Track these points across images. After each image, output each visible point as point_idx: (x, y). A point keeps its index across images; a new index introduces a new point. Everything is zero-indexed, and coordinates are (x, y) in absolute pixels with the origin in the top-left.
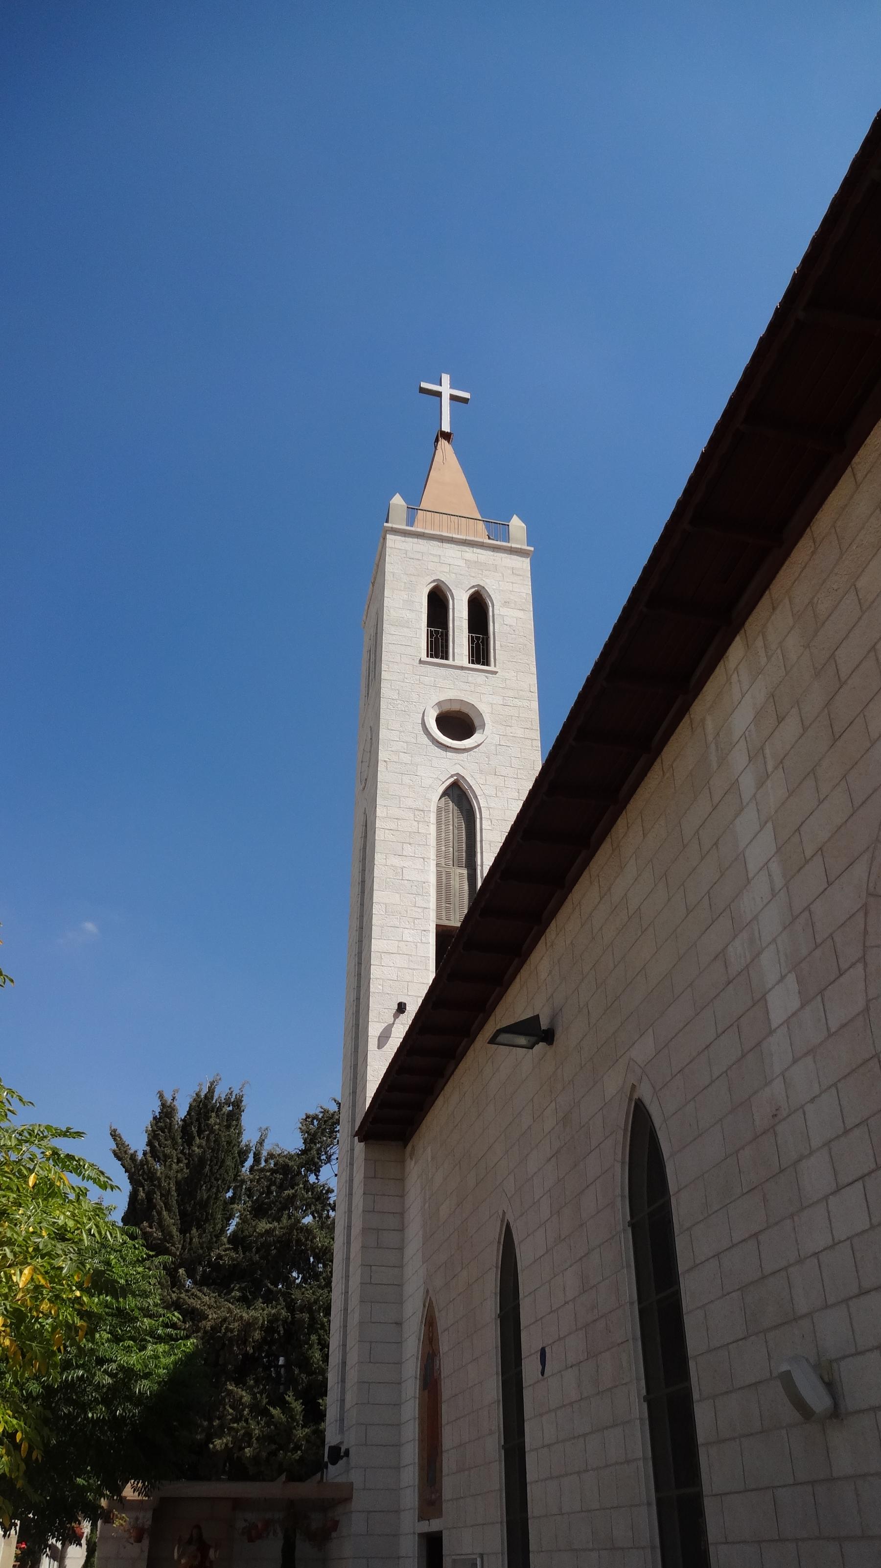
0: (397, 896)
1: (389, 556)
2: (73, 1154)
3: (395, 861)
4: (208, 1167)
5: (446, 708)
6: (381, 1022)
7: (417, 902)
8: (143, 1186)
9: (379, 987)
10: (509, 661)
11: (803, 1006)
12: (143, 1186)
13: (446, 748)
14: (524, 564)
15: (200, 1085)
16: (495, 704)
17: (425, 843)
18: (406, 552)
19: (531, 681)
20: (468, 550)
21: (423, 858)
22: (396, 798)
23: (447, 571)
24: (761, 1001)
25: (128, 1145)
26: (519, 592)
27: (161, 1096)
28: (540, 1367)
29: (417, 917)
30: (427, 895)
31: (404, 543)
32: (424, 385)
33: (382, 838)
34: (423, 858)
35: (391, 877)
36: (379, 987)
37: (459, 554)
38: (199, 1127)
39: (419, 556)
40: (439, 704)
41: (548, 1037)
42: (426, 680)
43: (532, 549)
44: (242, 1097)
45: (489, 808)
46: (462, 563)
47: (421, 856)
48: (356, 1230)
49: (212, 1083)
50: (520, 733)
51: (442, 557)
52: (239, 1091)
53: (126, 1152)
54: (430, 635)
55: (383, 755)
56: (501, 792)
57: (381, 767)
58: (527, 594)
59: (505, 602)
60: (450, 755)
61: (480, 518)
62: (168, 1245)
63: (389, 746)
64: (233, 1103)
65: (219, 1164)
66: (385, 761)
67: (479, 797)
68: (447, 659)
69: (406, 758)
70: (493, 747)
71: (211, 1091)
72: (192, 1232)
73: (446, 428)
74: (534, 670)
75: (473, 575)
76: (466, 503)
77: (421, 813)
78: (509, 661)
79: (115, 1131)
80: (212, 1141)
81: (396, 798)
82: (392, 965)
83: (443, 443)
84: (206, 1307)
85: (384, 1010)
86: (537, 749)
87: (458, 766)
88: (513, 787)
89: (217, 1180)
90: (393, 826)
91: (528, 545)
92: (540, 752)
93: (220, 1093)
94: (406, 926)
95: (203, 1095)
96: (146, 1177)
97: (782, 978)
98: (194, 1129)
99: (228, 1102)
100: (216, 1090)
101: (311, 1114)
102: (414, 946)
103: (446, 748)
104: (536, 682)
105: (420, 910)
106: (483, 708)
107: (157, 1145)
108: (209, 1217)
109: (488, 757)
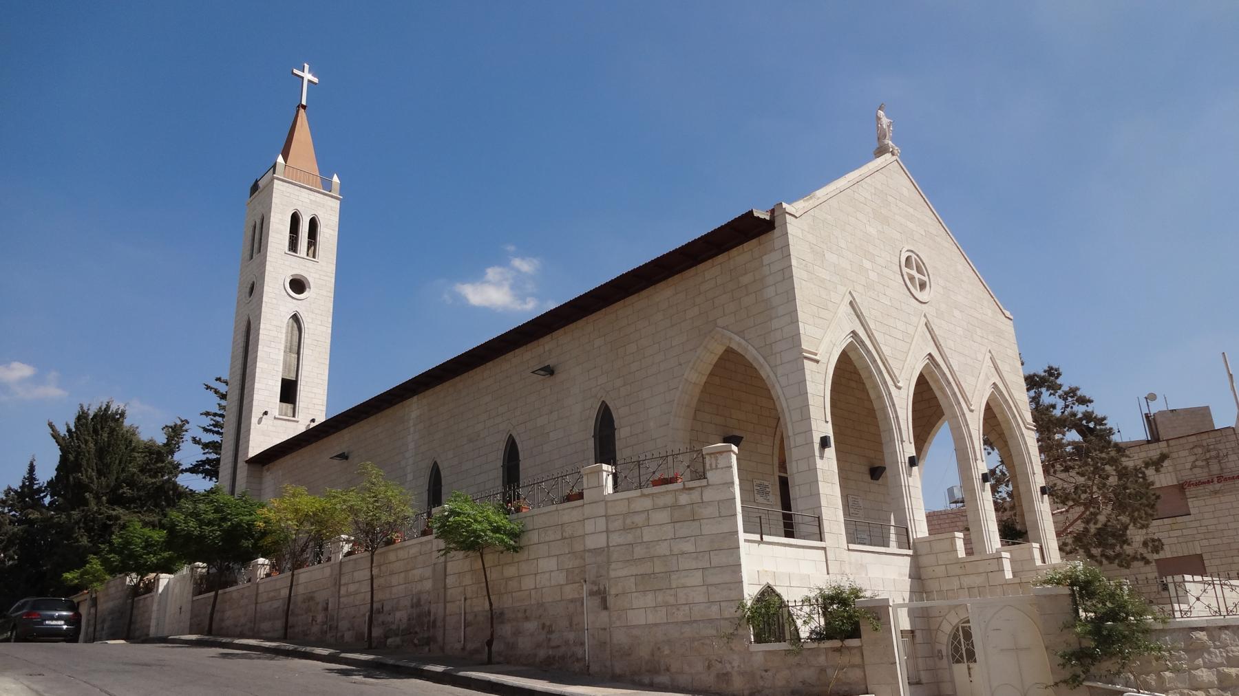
3: (266, 349)
5: (295, 277)
14: (336, 204)
18: (283, 192)
19: (332, 268)
24: (406, 475)
27: (82, 407)
32: (296, 71)
37: (307, 196)
39: (288, 195)
42: (286, 263)
46: (308, 201)
50: (325, 293)
54: (291, 237)
55: (265, 299)
57: (264, 305)
60: (294, 301)
64: (120, 414)
68: (297, 253)
71: (108, 407)
73: (304, 103)
76: (314, 168)
79: (51, 423)
83: (302, 111)
89: (115, 454)
93: (113, 408)
95: (103, 409)
98: (99, 427)
106: (310, 280)
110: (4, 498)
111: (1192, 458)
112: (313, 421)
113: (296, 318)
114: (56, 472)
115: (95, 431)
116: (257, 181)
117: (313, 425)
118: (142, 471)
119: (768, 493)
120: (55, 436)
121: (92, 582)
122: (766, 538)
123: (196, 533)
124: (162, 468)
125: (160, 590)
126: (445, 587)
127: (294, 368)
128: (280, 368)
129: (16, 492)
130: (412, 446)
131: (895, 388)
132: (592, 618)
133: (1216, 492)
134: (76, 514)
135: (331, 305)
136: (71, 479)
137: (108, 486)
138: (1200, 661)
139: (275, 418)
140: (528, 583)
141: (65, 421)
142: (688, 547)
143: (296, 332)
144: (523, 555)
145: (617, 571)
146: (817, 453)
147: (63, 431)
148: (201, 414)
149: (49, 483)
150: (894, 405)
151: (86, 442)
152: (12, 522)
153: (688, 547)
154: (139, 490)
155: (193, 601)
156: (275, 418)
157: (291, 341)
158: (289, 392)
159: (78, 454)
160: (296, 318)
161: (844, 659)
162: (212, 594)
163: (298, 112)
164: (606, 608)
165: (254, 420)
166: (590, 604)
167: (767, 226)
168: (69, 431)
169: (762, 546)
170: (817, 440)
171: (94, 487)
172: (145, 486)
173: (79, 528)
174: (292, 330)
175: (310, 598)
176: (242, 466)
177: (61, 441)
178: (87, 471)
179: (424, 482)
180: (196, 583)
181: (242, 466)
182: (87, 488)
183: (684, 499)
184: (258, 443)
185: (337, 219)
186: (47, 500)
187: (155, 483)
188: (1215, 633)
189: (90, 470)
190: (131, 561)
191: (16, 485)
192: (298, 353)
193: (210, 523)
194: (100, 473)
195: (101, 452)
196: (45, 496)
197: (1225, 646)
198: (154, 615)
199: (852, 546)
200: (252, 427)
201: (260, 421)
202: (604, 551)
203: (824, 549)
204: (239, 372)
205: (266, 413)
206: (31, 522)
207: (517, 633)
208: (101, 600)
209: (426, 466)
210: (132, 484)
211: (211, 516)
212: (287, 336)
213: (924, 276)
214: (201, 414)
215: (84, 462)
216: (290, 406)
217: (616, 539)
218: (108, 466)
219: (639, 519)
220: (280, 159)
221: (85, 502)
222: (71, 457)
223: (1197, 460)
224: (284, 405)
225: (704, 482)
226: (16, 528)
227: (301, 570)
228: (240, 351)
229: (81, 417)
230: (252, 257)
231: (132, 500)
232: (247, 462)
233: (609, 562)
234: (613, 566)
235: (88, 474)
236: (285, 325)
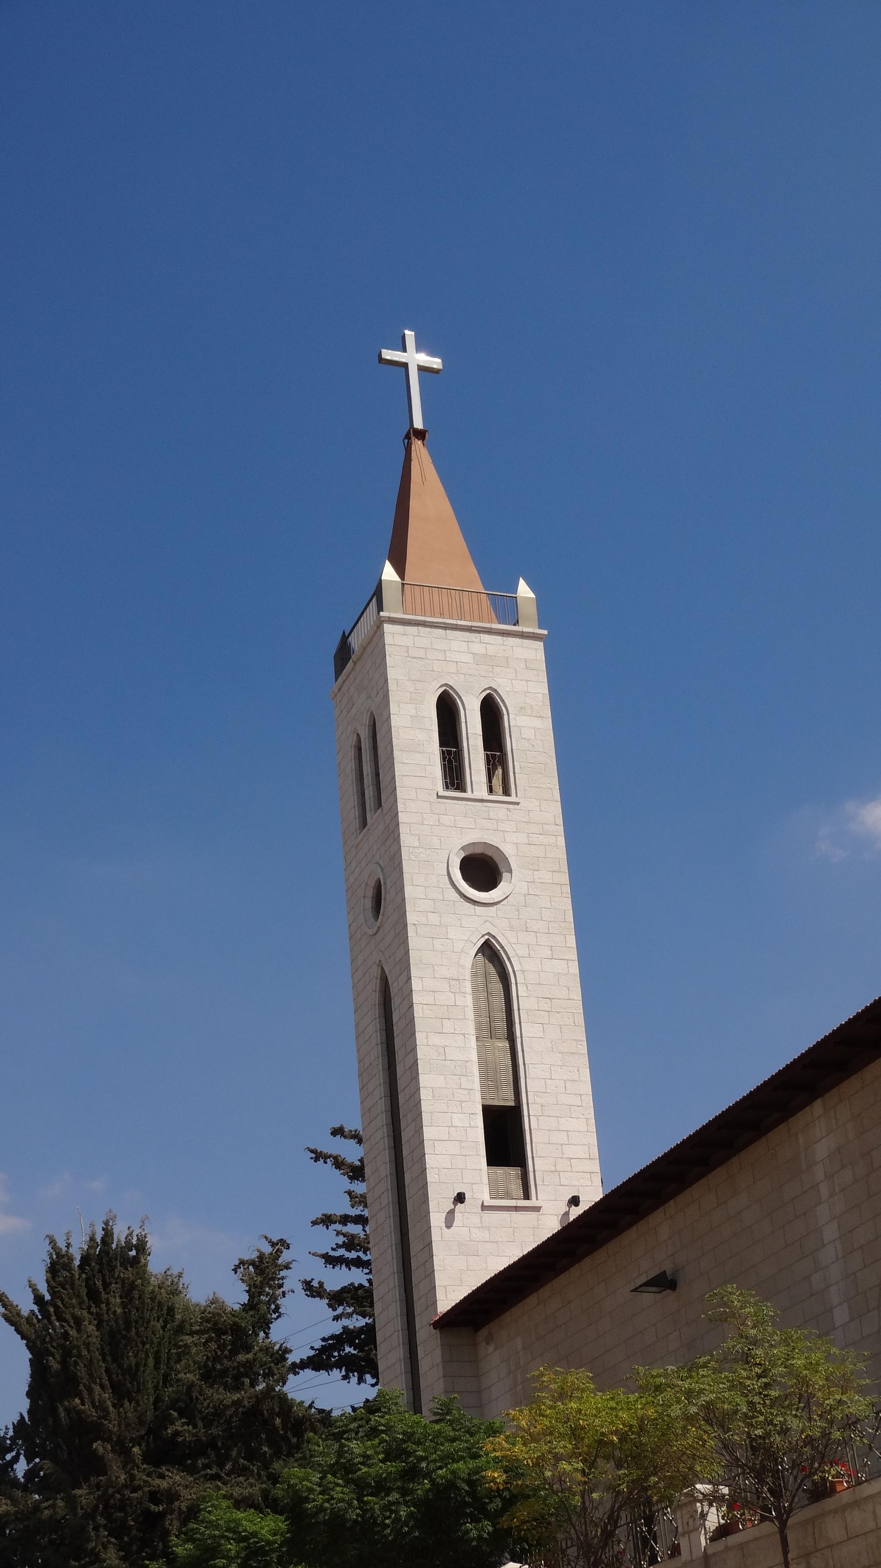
0: (443, 1078)
1: (389, 656)
2: (15, 1332)
3: (435, 1040)
4: (133, 1329)
6: (440, 1212)
7: (462, 1084)
8: (53, 1355)
9: (436, 1176)
10: (530, 787)
11: (850, 1321)
12: (53, 1355)
13: (475, 902)
14: (535, 652)
15: (92, 1225)
16: (519, 844)
17: (462, 1017)
20: (475, 640)
21: (464, 1035)
22: (428, 967)
23: (454, 671)
25: (17, 1306)
26: (535, 693)
27: (53, 1242)
29: (464, 1100)
30: (471, 1075)
31: (404, 637)
32: (388, 354)
33: (421, 1015)
34: (464, 1035)
35: (434, 1058)
36: (436, 1176)
38: (104, 1281)
39: (421, 654)
40: (463, 848)
42: (446, 820)
43: (545, 632)
44: (145, 1237)
45: (523, 971)
46: (469, 658)
47: (460, 1032)
49: (106, 1223)
51: (447, 654)
52: (140, 1230)
53: (18, 1314)
54: (445, 756)
55: (411, 918)
56: (534, 951)
58: (543, 694)
59: (521, 708)
60: (479, 909)
61: (484, 591)
62: (105, 1423)
63: (416, 905)
65: (145, 1325)
66: (414, 924)
67: (511, 959)
68: (465, 791)
69: (434, 919)
70: (522, 898)
72: (125, 1406)
73: (418, 424)
75: (483, 674)
77: (456, 982)
78: (530, 787)
80: (137, 1298)
81: (428, 967)
82: (445, 1152)
84: (180, 1488)
85: (443, 1200)
86: (567, 895)
87: (488, 924)
88: (546, 944)
90: (431, 1001)
91: (540, 627)
92: (570, 899)
93: (120, 1234)
94: (455, 1111)
96: (55, 1344)
97: (840, 1304)
98: (99, 1283)
99: (129, 1246)
100: (114, 1231)
101: (246, 1259)
102: (464, 1131)
103: (475, 902)
104: (561, 812)
105: (465, 1092)
106: (508, 850)
107: (61, 1305)
108: (141, 1387)
109: (518, 910)
112: (574, 1201)
114: (23, 1405)
117: (575, 1212)
118: (208, 1375)
123: (352, 1515)
124: (249, 1364)
128: (475, 1082)
130: (830, 1232)
135: (566, 904)
137: (141, 1422)
139: (484, 1207)
147: (26, 1305)
148: (314, 1223)
151: (78, 1322)
159: (67, 1353)
165: (437, 1219)
168: (39, 1299)
177: (25, 1327)
178: (90, 1391)
181: (424, 1332)
182: (97, 1431)
186: (21, 1467)
187: (237, 1403)
189: (97, 1389)
193: (381, 1487)
194: (120, 1393)
196: (16, 1459)
205: (460, 1198)
212: (476, 1000)
214: (314, 1223)
215: (81, 1371)
216: (513, 1172)
220: (389, 573)
221: (99, 1466)
222: (54, 1364)
224: (500, 1171)
230: (364, 823)
231: (199, 1449)
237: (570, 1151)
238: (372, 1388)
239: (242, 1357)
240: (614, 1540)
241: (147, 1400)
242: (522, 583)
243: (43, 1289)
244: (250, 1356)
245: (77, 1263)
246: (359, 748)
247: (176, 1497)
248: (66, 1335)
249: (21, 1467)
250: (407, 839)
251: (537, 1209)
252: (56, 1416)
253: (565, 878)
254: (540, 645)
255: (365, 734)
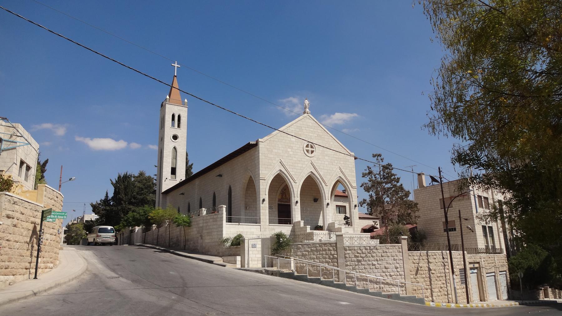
3: (166, 159)
14: (186, 109)
28: (188, 157)
32: (172, 64)
41: (184, 194)
42: (171, 131)
48: (160, 202)
55: (165, 143)
69: (168, 143)
71: (127, 174)
73: (176, 75)
74: (186, 128)
93: (128, 174)
99: (129, 175)
106: (178, 135)
110: (100, 203)
111: (454, 188)
112: (181, 180)
113: (175, 148)
114: (113, 195)
115: (124, 182)
116: (163, 103)
117: (181, 181)
118: (137, 194)
119: (273, 208)
120: (112, 183)
121: (122, 229)
122: (240, 224)
123: (139, 218)
124: (143, 193)
125: (136, 231)
126: (181, 234)
127: (175, 164)
128: (171, 164)
129: (103, 200)
130: (196, 192)
131: (294, 183)
132: (200, 241)
133: (459, 200)
134: (119, 208)
135: (186, 143)
136: (118, 197)
137: (128, 199)
138: (299, 251)
139: (170, 180)
140: (192, 233)
141: (115, 178)
142: (215, 227)
143: (175, 152)
144: (191, 227)
145: (204, 231)
146: (261, 203)
147: (114, 182)
149: (112, 198)
150: (293, 188)
151: (121, 185)
152: (102, 210)
153: (215, 227)
154: (137, 200)
155: (142, 235)
156: (170, 180)
157: (174, 155)
158: (173, 171)
159: (119, 189)
160: (175, 148)
161: (237, 250)
162: (145, 233)
163: (174, 78)
164: (202, 239)
165: (163, 181)
166: (200, 238)
167: (256, 145)
168: (116, 181)
169: (239, 225)
170: (261, 199)
171: (124, 199)
172: (138, 199)
173: (121, 212)
174: (174, 152)
175: (162, 235)
176: (161, 195)
177: (114, 185)
178: (122, 194)
179: (199, 203)
180: (143, 230)
181: (161, 194)
182: (122, 200)
183: (215, 217)
184: (165, 188)
185: (187, 114)
186: (112, 203)
187: (141, 198)
188: (303, 245)
189: (122, 194)
190: (129, 224)
191: (103, 198)
192: (176, 159)
193: (142, 216)
194: (125, 195)
195: (125, 188)
196: (111, 202)
197: (304, 248)
198: (135, 238)
199: (270, 225)
200: (163, 183)
201: (165, 180)
202: (202, 227)
203: (260, 225)
204: (159, 163)
205: (167, 178)
206: (108, 210)
207: (190, 244)
208: (125, 234)
209: (199, 198)
210: (135, 198)
211: (143, 214)
212: (172, 154)
213: (314, 149)
215: (121, 192)
216: (174, 176)
217: (204, 225)
218: (128, 192)
219: (208, 220)
220: (168, 97)
221: (122, 204)
222: (117, 190)
223: (455, 189)
224: (172, 175)
225: (218, 213)
226: (104, 212)
227: (160, 228)
228: (160, 159)
229: (119, 177)
230: (161, 129)
231: (135, 203)
232: (162, 193)
233: (203, 230)
234: (204, 230)
235: (122, 196)
236: (171, 151)
237: (182, 174)
238: (59, 254)
239: (142, 192)
240: (557, 143)
241: (129, 196)
242: (186, 99)
243: (117, 180)
244: (143, 192)
245: (122, 177)
246: (162, 118)
247: (131, 209)
248: (119, 187)
249: (112, 203)
250: (166, 133)
251: (176, 180)
252: (117, 197)
253: (186, 139)
254: (187, 108)
255: (163, 117)
